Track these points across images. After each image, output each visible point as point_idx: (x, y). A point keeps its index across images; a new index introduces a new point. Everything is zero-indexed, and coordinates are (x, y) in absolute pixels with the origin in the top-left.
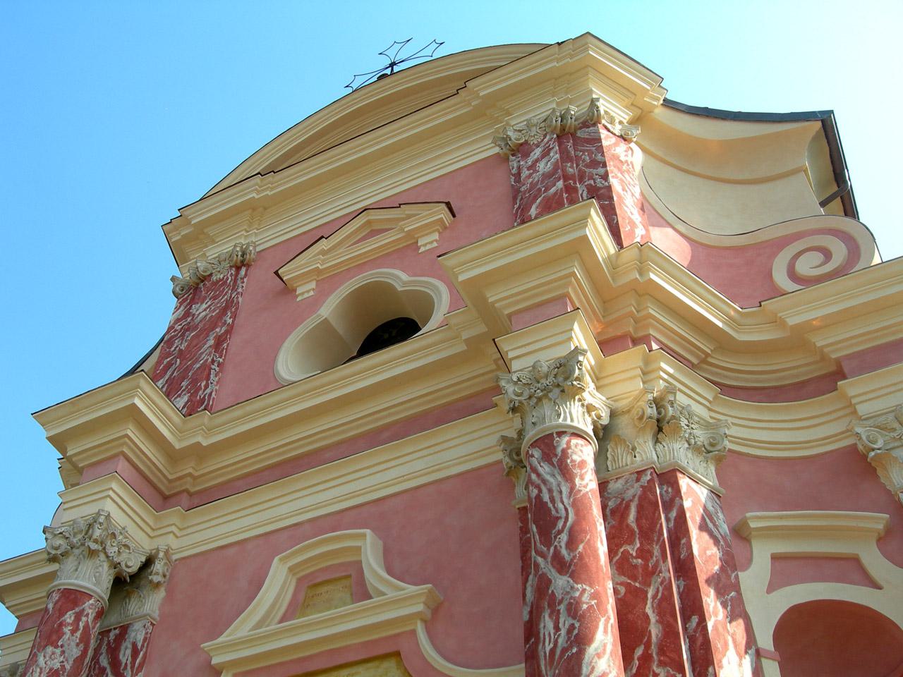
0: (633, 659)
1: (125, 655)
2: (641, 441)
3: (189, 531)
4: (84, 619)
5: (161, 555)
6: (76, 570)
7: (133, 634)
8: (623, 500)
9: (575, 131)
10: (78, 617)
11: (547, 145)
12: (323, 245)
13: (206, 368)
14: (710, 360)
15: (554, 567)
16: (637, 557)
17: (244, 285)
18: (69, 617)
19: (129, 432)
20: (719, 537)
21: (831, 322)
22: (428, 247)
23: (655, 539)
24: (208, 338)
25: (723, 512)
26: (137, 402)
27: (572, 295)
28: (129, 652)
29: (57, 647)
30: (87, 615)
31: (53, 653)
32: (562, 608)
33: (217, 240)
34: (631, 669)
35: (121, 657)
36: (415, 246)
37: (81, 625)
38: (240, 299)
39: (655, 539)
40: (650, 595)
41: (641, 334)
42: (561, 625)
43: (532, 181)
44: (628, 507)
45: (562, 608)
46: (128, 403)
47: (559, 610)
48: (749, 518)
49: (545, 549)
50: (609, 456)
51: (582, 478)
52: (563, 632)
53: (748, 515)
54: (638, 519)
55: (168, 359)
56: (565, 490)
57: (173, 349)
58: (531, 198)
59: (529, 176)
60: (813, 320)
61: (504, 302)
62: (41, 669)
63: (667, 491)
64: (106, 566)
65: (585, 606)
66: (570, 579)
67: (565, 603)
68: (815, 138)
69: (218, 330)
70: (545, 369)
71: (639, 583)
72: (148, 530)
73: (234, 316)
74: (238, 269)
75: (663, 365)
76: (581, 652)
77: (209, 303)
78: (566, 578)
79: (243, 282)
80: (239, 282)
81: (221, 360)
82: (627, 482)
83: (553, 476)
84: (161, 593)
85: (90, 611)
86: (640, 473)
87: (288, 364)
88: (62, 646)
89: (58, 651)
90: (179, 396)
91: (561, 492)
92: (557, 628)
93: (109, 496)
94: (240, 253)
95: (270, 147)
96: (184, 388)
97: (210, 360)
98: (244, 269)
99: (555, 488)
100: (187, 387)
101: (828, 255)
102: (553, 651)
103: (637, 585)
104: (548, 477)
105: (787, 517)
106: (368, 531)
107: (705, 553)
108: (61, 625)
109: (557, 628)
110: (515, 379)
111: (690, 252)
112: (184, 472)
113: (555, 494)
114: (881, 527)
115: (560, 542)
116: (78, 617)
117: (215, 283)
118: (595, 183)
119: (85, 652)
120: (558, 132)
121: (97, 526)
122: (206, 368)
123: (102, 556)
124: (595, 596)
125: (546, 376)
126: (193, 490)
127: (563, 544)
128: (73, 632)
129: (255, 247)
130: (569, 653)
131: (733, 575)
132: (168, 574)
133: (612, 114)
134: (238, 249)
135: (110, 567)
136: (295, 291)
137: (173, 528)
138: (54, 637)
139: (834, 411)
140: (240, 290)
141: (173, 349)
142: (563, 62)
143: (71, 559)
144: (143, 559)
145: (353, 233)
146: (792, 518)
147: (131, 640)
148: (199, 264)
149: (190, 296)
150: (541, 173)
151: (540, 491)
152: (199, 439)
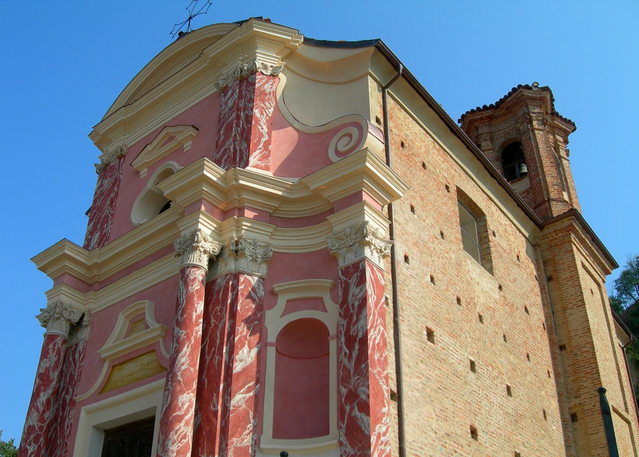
1: (77, 356)
2: (229, 260)
3: (98, 300)
5: (86, 313)
6: (52, 326)
10: (54, 346)
12: (149, 148)
13: (107, 217)
14: (279, 209)
17: (123, 168)
18: (51, 346)
19: (66, 264)
20: (256, 298)
21: (329, 186)
22: (188, 148)
26: (66, 251)
27: (205, 197)
28: (78, 355)
29: (47, 358)
30: (58, 344)
31: (46, 361)
32: (175, 340)
33: (113, 141)
36: (182, 148)
37: (56, 348)
38: (121, 176)
40: (220, 327)
41: (241, 206)
45: (175, 340)
46: (62, 253)
48: (275, 287)
51: (192, 286)
53: (274, 286)
56: (184, 292)
60: (322, 186)
61: (182, 203)
64: (64, 322)
65: (181, 339)
68: (373, 55)
69: (111, 196)
70: (188, 237)
72: (82, 302)
73: (118, 187)
74: (120, 158)
75: (244, 223)
76: (177, 356)
78: (178, 328)
79: (122, 167)
80: (120, 166)
81: (112, 212)
83: (182, 286)
84: (89, 329)
85: (59, 342)
86: (227, 275)
87: (137, 216)
89: (48, 360)
90: (97, 232)
93: (61, 293)
94: (120, 151)
95: (129, 87)
97: (108, 212)
98: (122, 159)
101: (350, 135)
105: (292, 284)
106: (146, 301)
108: (48, 349)
110: (178, 242)
111: (297, 139)
112: (94, 274)
114: (329, 285)
116: (54, 346)
117: (111, 168)
119: (59, 359)
120: (239, 79)
121: (57, 307)
122: (107, 217)
123: (62, 319)
124: (187, 334)
125: (189, 240)
126: (100, 281)
128: (53, 352)
129: (126, 147)
132: (90, 320)
133: (265, 63)
134: (118, 149)
135: (66, 322)
136: (140, 172)
137: (92, 300)
138: (46, 355)
139: (328, 229)
140: (121, 171)
142: (249, 32)
143: (51, 321)
144: (81, 315)
145: (159, 143)
146: (295, 284)
148: (104, 158)
152: (96, 260)
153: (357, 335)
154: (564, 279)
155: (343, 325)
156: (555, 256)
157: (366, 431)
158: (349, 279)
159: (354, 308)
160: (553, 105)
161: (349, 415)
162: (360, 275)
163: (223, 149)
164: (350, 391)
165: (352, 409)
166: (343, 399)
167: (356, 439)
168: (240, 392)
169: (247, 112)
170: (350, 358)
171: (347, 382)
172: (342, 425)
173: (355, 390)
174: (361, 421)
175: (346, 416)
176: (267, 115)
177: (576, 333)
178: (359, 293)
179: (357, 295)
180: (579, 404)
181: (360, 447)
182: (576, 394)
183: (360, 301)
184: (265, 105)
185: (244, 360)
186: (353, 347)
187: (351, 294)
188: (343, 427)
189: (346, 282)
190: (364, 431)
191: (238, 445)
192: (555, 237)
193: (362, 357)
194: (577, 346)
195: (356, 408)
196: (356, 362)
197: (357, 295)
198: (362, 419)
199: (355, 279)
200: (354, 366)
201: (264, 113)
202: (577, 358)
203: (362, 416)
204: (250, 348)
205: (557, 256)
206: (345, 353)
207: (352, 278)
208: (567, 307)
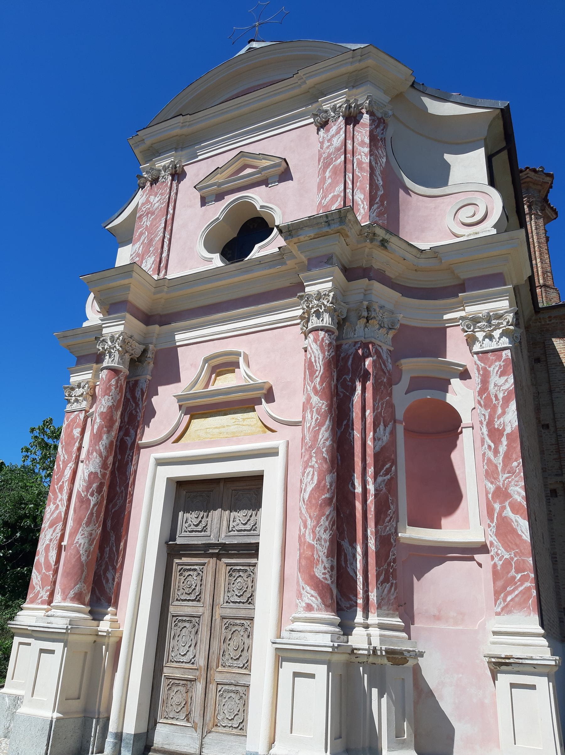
0: (342, 425)
1: (138, 394)
4: (120, 382)
7: (141, 385)
8: (347, 354)
9: (356, 116)
11: (340, 125)
15: (313, 392)
16: (349, 382)
20: (386, 372)
23: (358, 374)
24: (161, 222)
25: (391, 359)
28: (140, 393)
34: (341, 429)
35: (136, 395)
37: (119, 385)
39: (358, 374)
42: (313, 417)
43: (329, 151)
44: (349, 358)
45: (314, 410)
47: (313, 411)
49: (311, 383)
50: (344, 332)
52: (314, 420)
54: (352, 364)
55: (141, 230)
57: (142, 223)
58: (327, 164)
59: (328, 147)
62: (104, 406)
63: (366, 352)
66: (318, 398)
67: (316, 408)
71: (349, 393)
77: (159, 198)
82: (350, 346)
88: (112, 395)
90: (149, 256)
91: (319, 358)
92: (312, 418)
96: (151, 252)
99: (317, 356)
100: (153, 252)
102: (309, 427)
103: (348, 394)
104: (315, 350)
107: (378, 381)
109: (312, 418)
113: (317, 359)
115: (316, 381)
118: (361, 158)
127: (317, 382)
130: (315, 429)
131: (390, 389)
141: (142, 223)
147: (140, 387)
149: (148, 188)
150: (334, 146)
151: (311, 356)
153: (504, 430)
154: (553, 364)
155: (484, 415)
156: (546, 340)
157: (523, 535)
158: (489, 367)
159: (497, 399)
160: (548, 192)
161: (500, 514)
162: (503, 365)
163: (332, 194)
164: (498, 489)
165: (503, 508)
166: (490, 496)
167: (511, 543)
168: (380, 474)
169: (360, 157)
170: (496, 452)
171: (495, 479)
172: (491, 524)
173: (506, 489)
174: (516, 524)
175: (496, 515)
176: (381, 165)
177: (561, 416)
178: (504, 384)
179: (501, 386)
180: (560, 482)
181: (517, 552)
182: (557, 472)
183: (506, 393)
184: (378, 152)
185: (381, 439)
186: (500, 442)
187: (493, 383)
188: (492, 526)
189: (485, 369)
190: (522, 536)
191: (383, 534)
192: (548, 322)
193: (512, 454)
194: (562, 428)
195: (508, 508)
196: (504, 458)
197: (501, 386)
198: (517, 521)
199: (497, 368)
200: (503, 461)
201: (378, 162)
202: (561, 439)
203: (517, 518)
204: (385, 426)
205: (547, 341)
206: (489, 447)
207: (493, 366)
208: (554, 390)
